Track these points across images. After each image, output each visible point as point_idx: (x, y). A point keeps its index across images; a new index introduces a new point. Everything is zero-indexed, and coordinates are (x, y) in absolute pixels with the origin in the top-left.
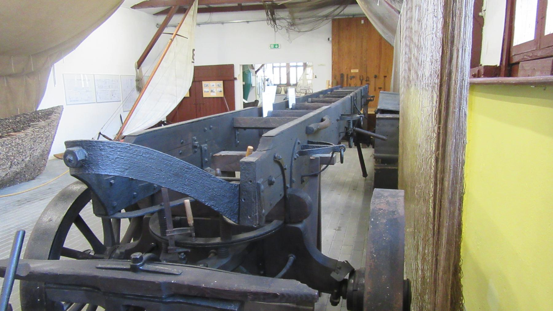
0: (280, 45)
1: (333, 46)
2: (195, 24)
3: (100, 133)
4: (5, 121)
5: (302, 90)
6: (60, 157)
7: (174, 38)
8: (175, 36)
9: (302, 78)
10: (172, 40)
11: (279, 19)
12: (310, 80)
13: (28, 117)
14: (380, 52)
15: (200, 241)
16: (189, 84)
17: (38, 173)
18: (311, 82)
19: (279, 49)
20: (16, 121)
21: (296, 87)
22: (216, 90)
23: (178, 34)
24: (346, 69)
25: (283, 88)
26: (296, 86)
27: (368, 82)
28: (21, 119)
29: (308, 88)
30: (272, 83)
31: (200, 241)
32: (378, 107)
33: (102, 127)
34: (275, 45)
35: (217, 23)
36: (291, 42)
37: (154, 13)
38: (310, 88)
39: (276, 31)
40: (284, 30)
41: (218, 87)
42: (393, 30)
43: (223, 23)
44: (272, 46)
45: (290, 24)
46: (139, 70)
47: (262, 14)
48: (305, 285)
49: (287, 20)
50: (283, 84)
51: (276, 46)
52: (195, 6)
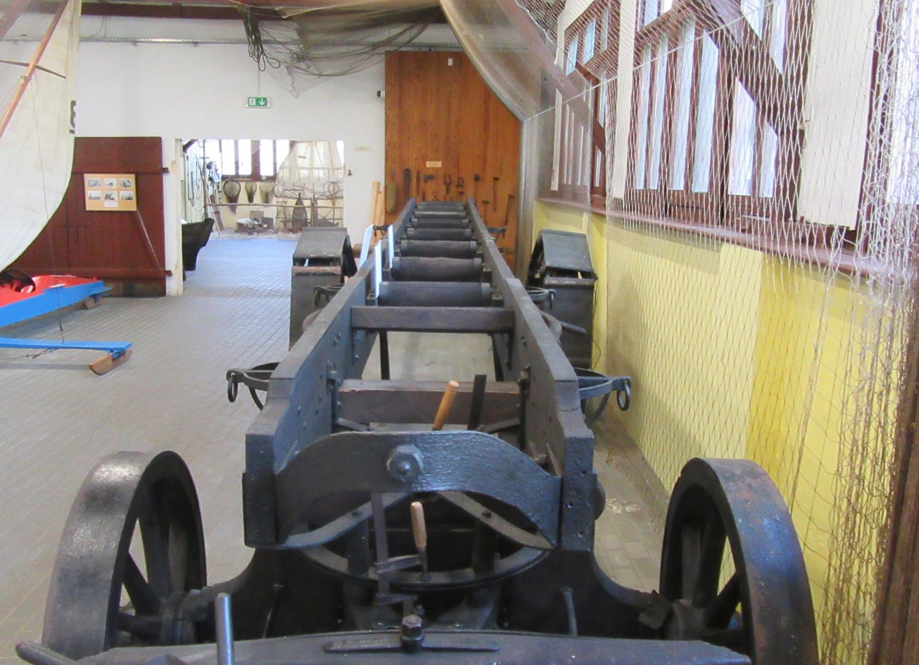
0: (271, 99)
1: (387, 109)
2: (76, 40)
5: (289, 190)
7: (30, 75)
8: (33, 71)
9: (287, 164)
10: (27, 80)
14: (486, 124)
15: (439, 578)
21: (273, 183)
23: (40, 64)
24: (416, 159)
25: (243, 185)
26: (275, 182)
27: (460, 189)
29: (302, 187)
30: (218, 172)
31: (439, 578)
34: (258, 100)
35: (124, 40)
36: (298, 96)
39: (262, 69)
41: (124, 188)
43: (137, 42)
44: (252, 101)
45: (295, 56)
47: (238, 29)
48: (707, 643)
50: (243, 177)
51: (260, 102)
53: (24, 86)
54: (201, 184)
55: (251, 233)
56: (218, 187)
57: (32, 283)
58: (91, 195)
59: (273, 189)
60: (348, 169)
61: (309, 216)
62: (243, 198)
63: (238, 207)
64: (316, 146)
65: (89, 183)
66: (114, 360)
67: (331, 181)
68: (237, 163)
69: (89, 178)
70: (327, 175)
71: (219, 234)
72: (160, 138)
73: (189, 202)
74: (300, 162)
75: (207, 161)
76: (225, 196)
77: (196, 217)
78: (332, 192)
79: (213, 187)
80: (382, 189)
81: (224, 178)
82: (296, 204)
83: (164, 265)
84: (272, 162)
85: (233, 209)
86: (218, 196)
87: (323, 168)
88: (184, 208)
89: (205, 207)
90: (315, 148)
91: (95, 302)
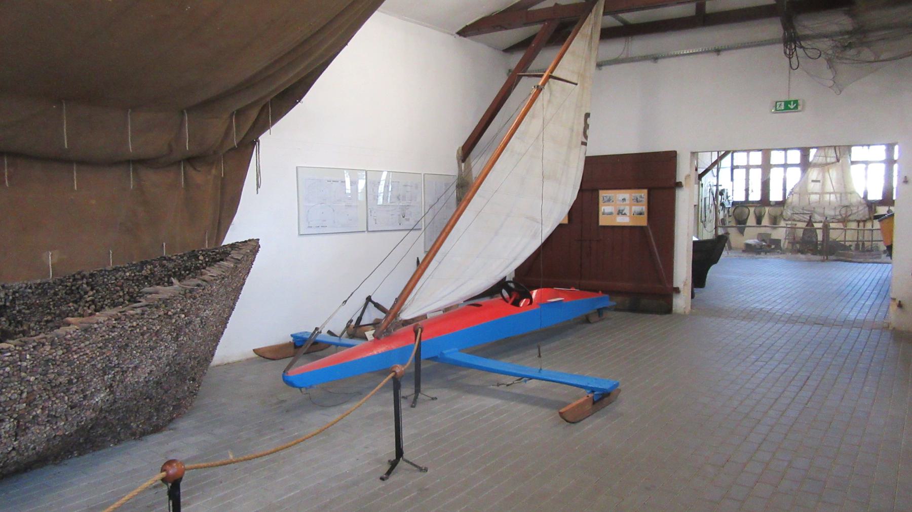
2: (594, 64)
3: (369, 299)
4: (114, 276)
5: (797, 214)
6: (268, 355)
7: (544, 84)
9: (797, 190)
10: (539, 89)
12: (816, 193)
13: (171, 265)
16: (569, 194)
17: (171, 413)
18: (818, 199)
19: (800, 113)
20: (142, 275)
21: (782, 208)
23: (554, 74)
25: (752, 210)
26: (784, 206)
28: (156, 269)
30: (729, 199)
33: (345, 300)
34: (787, 103)
35: (645, 58)
37: (505, 48)
38: (814, 212)
39: (794, 66)
41: (636, 203)
46: (465, 165)
50: (753, 202)
51: (790, 106)
52: (596, 20)
54: (713, 208)
55: (759, 253)
56: (728, 211)
58: (604, 210)
59: (782, 213)
61: (820, 238)
62: (752, 221)
63: (747, 229)
64: (829, 172)
65: (603, 198)
66: (594, 403)
67: (843, 204)
68: (747, 190)
70: (839, 199)
71: (728, 253)
72: (675, 152)
73: (701, 225)
75: (720, 188)
76: (734, 220)
77: (708, 234)
78: (844, 216)
79: (724, 212)
81: (734, 203)
82: (807, 226)
84: (781, 188)
85: (742, 231)
86: (728, 220)
87: (834, 193)
88: (696, 222)
89: (716, 228)
90: (827, 175)
91: (599, 316)
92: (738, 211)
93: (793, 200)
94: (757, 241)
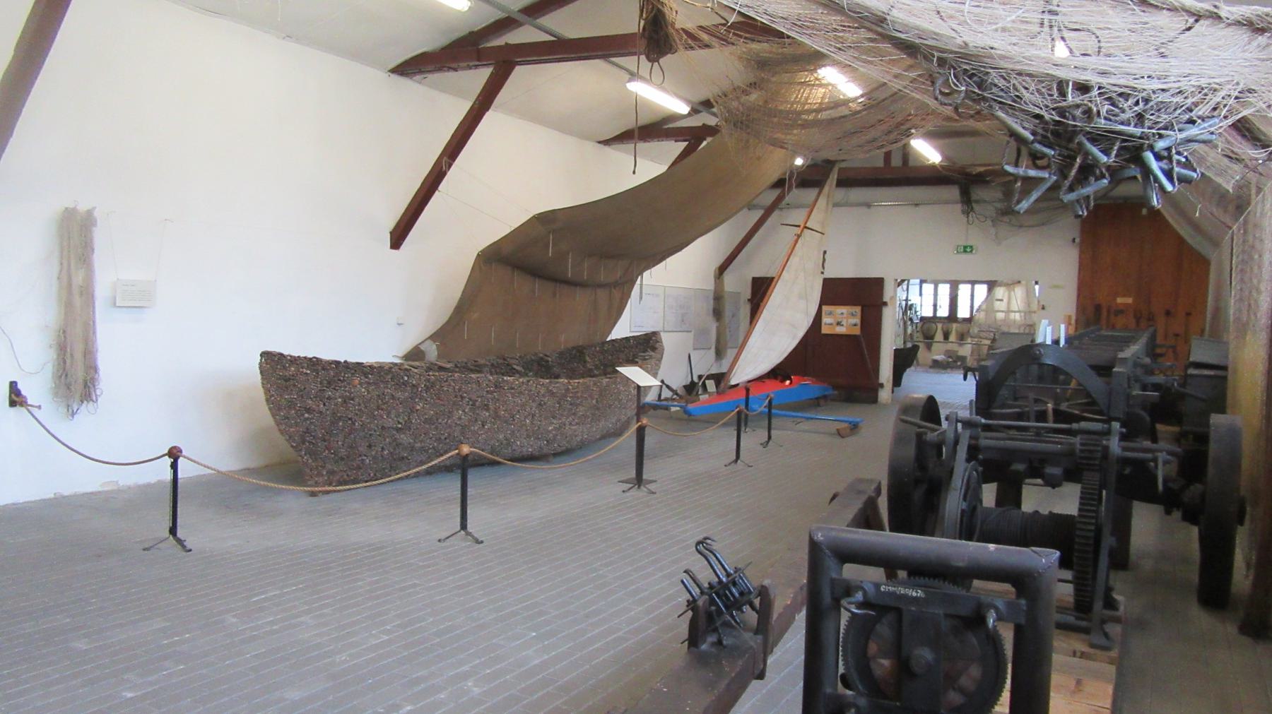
1: (1081, 253)
2: (830, 206)
9: (984, 307)
10: (799, 236)
11: (977, 202)
12: (1003, 311)
21: (969, 325)
22: (847, 321)
23: (807, 225)
25: (940, 326)
26: (971, 323)
27: (1078, 654)
30: (918, 314)
32: (1191, 359)
34: (965, 247)
40: (989, 222)
42: (1216, 244)
49: (994, 204)
51: (967, 249)
53: (796, 242)
57: (790, 379)
60: (1042, 303)
62: (939, 336)
63: (934, 344)
68: (935, 306)
69: (825, 308)
70: (1023, 318)
72: (883, 279)
74: (998, 305)
75: (910, 303)
76: (922, 336)
80: (1073, 322)
81: (923, 319)
83: (878, 378)
86: (916, 335)
87: (1019, 311)
90: (1012, 293)
92: (926, 326)
93: (981, 317)
94: (943, 357)
